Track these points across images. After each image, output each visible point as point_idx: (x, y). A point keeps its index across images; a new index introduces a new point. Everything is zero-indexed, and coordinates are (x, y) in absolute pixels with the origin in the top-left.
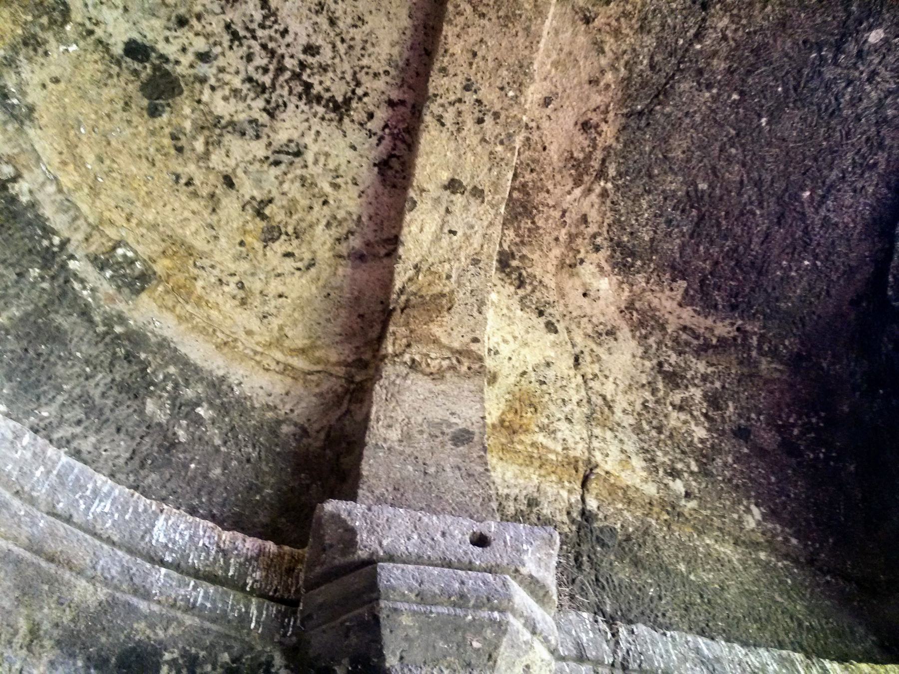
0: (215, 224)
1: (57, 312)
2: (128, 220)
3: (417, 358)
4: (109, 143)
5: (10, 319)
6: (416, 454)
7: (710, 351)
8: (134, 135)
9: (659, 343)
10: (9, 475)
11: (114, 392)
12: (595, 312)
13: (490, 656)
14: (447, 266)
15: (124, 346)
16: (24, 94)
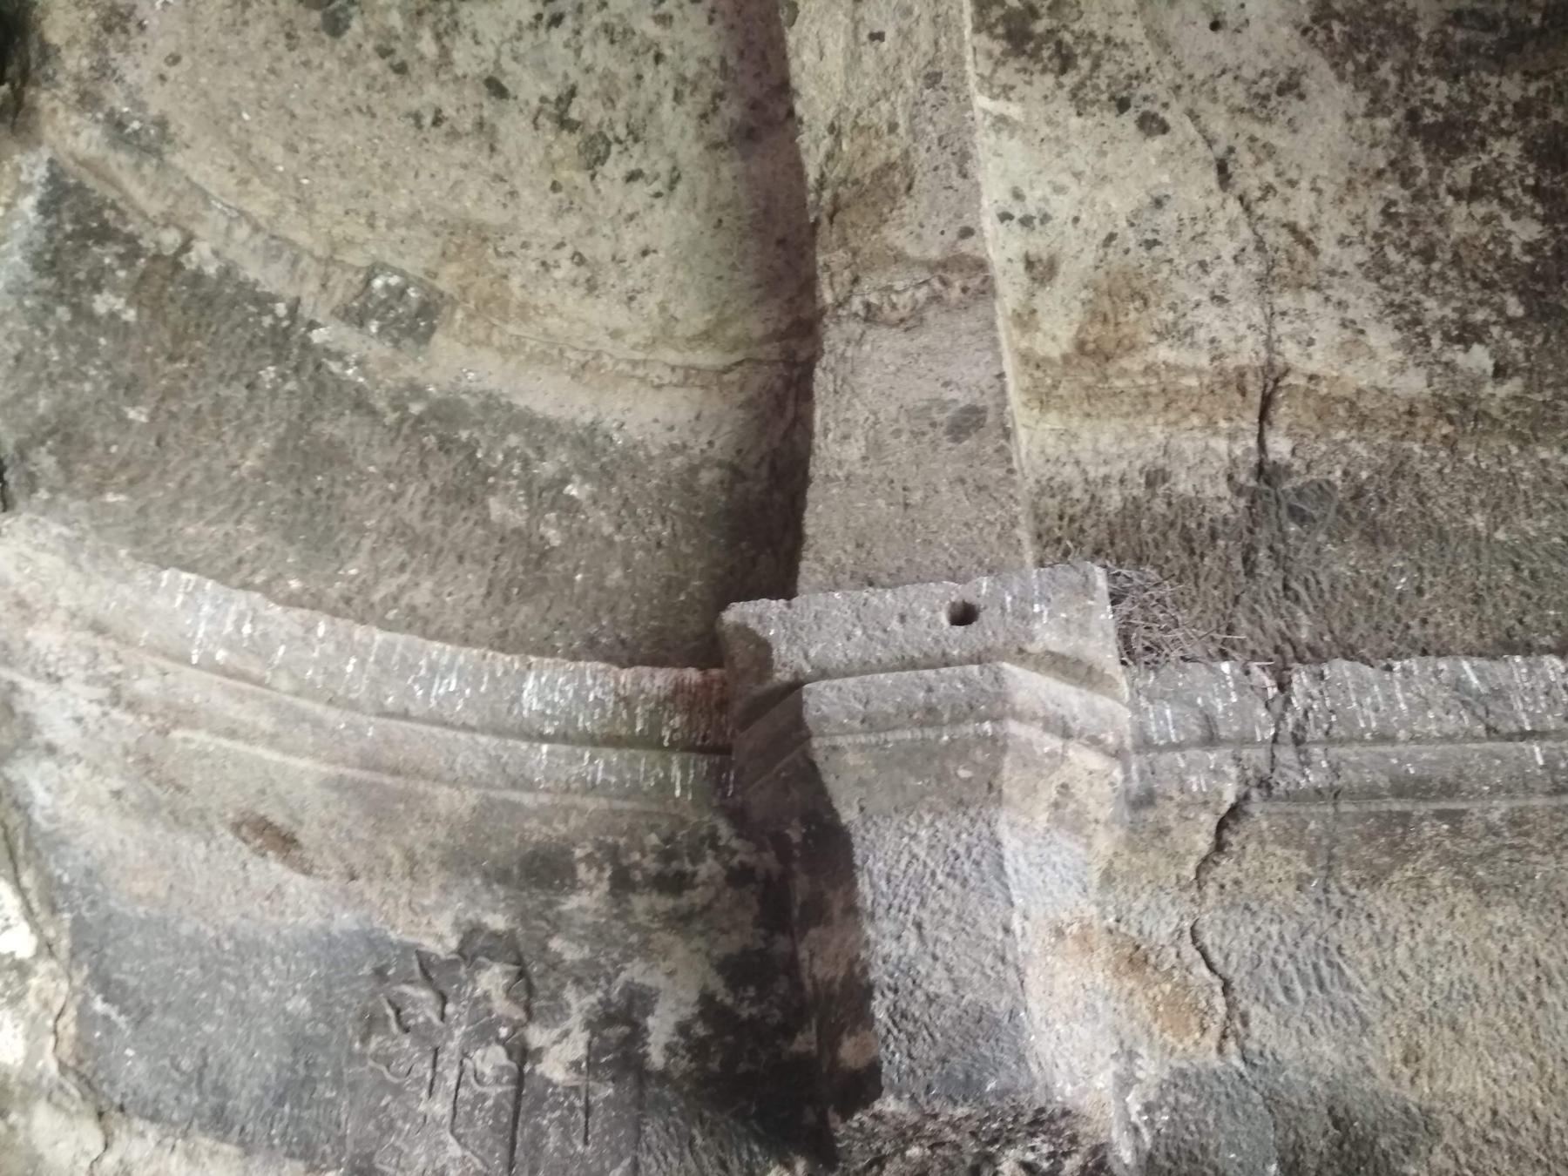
0: (503, 172)
1: (320, 419)
2: (372, 226)
3: (873, 299)
4: (293, 116)
5: (261, 456)
6: (891, 474)
7: (1530, 46)
8: (325, 80)
9: (1403, 71)
10: (312, 682)
11: (438, 506)
12: (1244, 54)
13: (990, 786)
14: (884, 106)
15: (433, 431)
16: (141, 106)
